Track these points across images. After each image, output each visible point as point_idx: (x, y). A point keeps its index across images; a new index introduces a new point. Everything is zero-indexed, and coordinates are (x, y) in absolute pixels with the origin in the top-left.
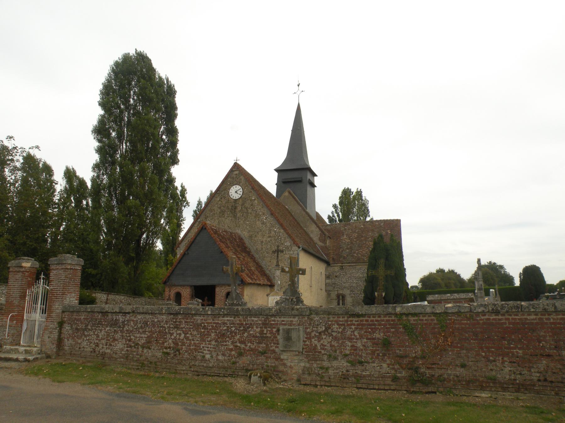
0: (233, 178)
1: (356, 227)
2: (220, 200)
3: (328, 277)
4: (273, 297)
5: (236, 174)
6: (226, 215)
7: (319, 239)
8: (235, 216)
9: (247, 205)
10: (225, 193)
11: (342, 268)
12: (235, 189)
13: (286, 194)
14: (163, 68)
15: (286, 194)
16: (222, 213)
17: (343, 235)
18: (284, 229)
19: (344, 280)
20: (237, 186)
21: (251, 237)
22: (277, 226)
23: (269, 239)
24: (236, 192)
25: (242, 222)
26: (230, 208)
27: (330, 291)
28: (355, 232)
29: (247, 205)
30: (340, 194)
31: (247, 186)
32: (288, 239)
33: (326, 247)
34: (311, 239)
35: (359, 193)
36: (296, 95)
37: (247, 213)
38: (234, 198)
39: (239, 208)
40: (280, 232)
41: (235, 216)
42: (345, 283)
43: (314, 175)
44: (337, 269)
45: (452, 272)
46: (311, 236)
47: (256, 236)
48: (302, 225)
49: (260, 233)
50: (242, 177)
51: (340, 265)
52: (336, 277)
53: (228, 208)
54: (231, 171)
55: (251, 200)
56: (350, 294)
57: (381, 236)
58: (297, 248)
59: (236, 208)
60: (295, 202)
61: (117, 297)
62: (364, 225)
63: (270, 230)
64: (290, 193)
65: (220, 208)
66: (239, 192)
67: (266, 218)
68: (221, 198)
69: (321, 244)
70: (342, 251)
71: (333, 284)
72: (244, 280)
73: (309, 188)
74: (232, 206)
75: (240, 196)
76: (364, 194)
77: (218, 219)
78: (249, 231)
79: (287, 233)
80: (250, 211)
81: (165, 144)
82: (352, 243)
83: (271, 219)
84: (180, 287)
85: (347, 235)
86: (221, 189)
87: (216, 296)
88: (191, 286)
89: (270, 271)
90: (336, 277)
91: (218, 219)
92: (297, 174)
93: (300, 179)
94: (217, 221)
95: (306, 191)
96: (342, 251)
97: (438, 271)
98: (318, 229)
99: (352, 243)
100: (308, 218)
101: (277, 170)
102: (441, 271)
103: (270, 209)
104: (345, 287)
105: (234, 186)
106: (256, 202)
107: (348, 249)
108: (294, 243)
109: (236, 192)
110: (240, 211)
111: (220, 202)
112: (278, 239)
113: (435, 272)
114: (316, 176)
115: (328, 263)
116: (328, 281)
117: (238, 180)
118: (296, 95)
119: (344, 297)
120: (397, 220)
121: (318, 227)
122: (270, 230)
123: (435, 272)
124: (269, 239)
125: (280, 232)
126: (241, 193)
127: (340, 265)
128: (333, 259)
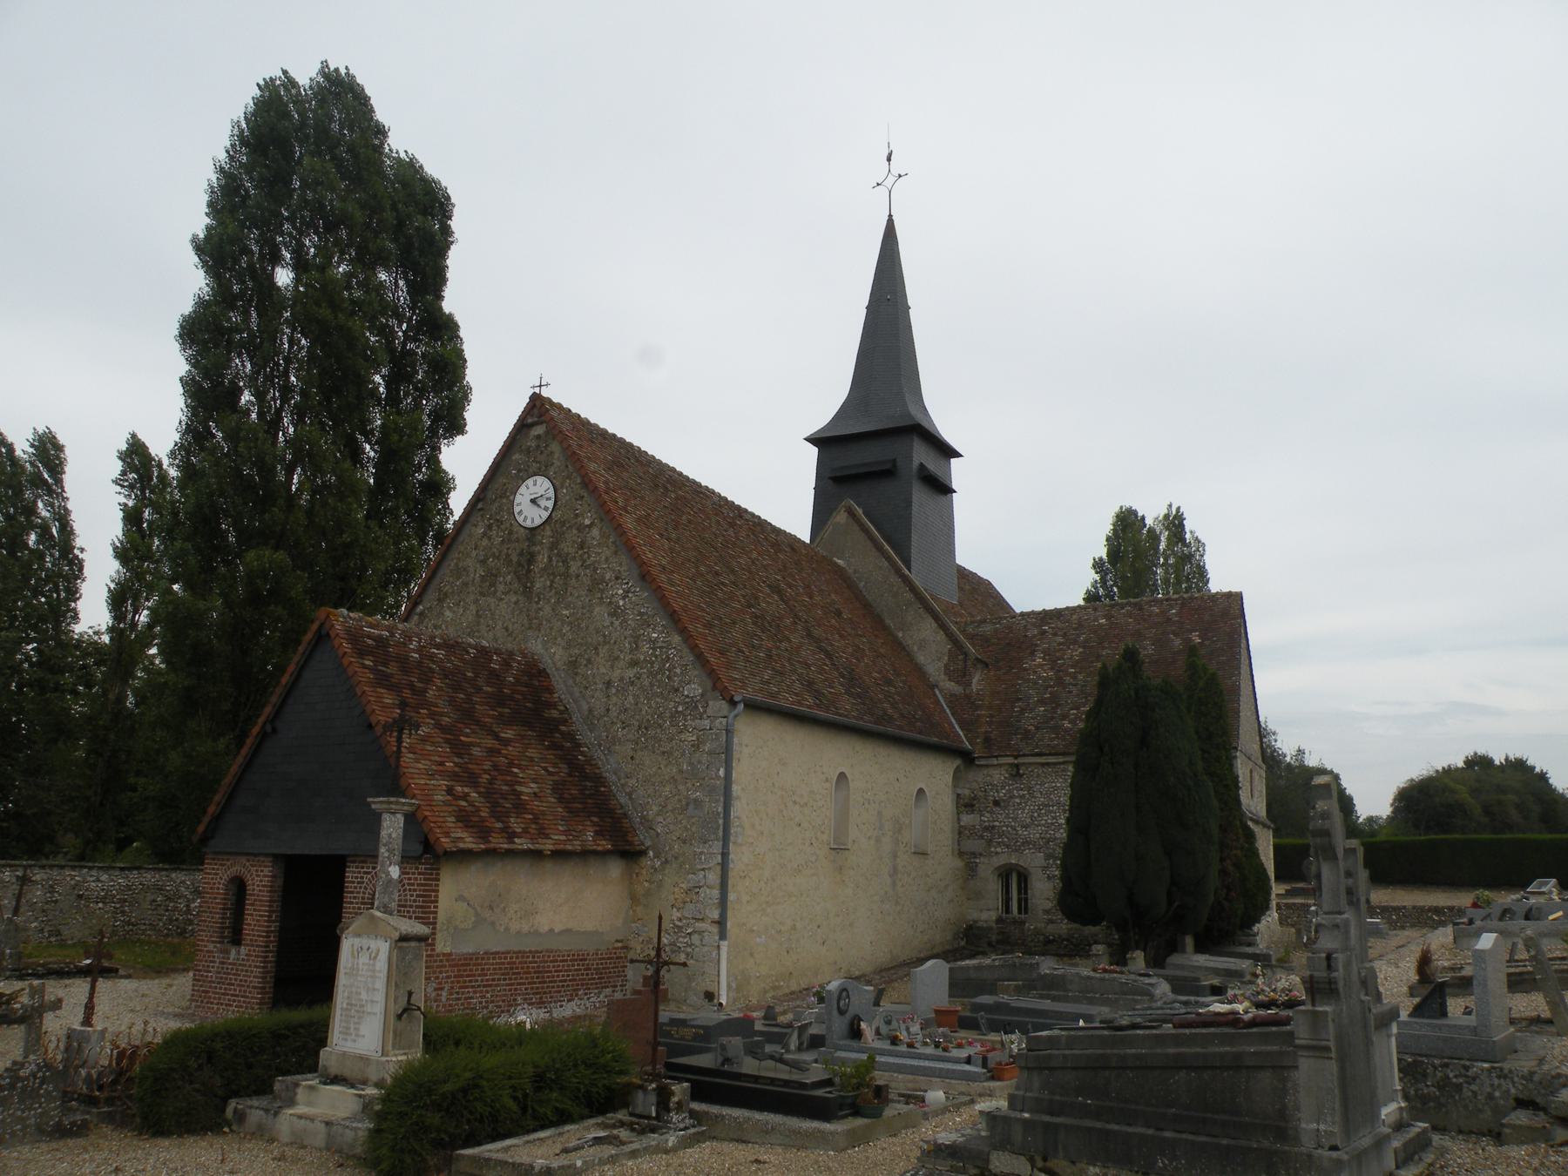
0: (528, 451)
1: (1080, 625)
2: (484, 534)
3: (966, 805)
4: (357, 941)
5: (538, 437)
6: (501, 588)
7: (948, 672)
8: (527, 592)
9: (567, 547)
10: (500, 509)
11: (1016, 773)
12: (533, 489)
13: (841, 517)
14: (416, 127)
15: (841, 517)
16: (491, 577)
17: (1032, 653)
18: (683, 631)
19: (1023, 815)
20: (540, 479)
21: (573, 664)
22: (660, 621)
23: (630, 673)
24: (533, 501)
25: (548, 609)
26: (515, 559)
27: (974, 855)
28: (1075, 642)
29: (567, 547)
30: (1107, 528)
31: (569, 477)
32: (695, 672)
33: (968, 697)
34: (919, 670)
35: (1175, 523)
36: (883, 191)
37: (566, 576)
38: (528, 524)
39: (542, 559)
40: (669, 645)
41: (527, 592)
42: (1026, 827)
43: (949, 452)
44: (998, 776)
45: (1518, 767)
46: (921, 658)
47: (589, 661)
48: (888, 622)
49: (603, 651)
50: (555, 447)
51: (1010, 760)
52: (996, 803)
53: (508, 562)
54: (522, 427)
55: (581, 528)
56: (1045, 868)
57: (1131, 656)
58: (724, 705)
59: (531, 559)
60: (869, 543)
61: (178, 876)
62: (1108, 617)
63: (636, 639)
64: (851, 513)
65: (483, 562)
66: (543, 503)
67: (627, 591)
68: (490, 527)
69: (950, 686)
70: (1023, 711)
71: (986, 829)
72: (432, 839)
73: (920, 496)
74: (521, 554)
75: (545, 515)
76: (1189, 525)
77: (476, 601)
78: (569, 645)
79: (694, 648)
80: (574, 567)
81: (252, 335)
82: (1060, 682)
83: (641, 594)
84: (243, 859)
85: (1046, 652)
86: (490, 495)
87: (348, 897)
88: (276, 857)
89: (630, 795)
90: (996, 803)
91: (476, 601)
92: (883, 453)
93: (888, 466)
94: (473, 608)
95: (908, 504)
96: (1023, 711)
97: (1468, 762)
98: (941, 636)
99: (1060, 682)
100: (909, 596)
101: (813, 440)
102: (1479, 763)
103: (636, 558)
104: (1026, 843)
105: (530, 482)
106: (595, 532)
107: (1042, 702)
108: (714, 688)
109: (533, 501)
110: (544, 569)
111: (485, 542)
112: (661, 670)
113: (1461, 764)
114: (958, 455)
115: (967, 758)
116: (967, 819)
117: (542, 458)
118: (883, 191)
119: (1024, 878)
120: (1229, 595)
121: (943, 626)
122: (636, 639)
123: (1461, 764)
124: (630, 673)
125: (669, 645)
126: (550, 504)
127: (1010, 760)
128: (987, 740)
